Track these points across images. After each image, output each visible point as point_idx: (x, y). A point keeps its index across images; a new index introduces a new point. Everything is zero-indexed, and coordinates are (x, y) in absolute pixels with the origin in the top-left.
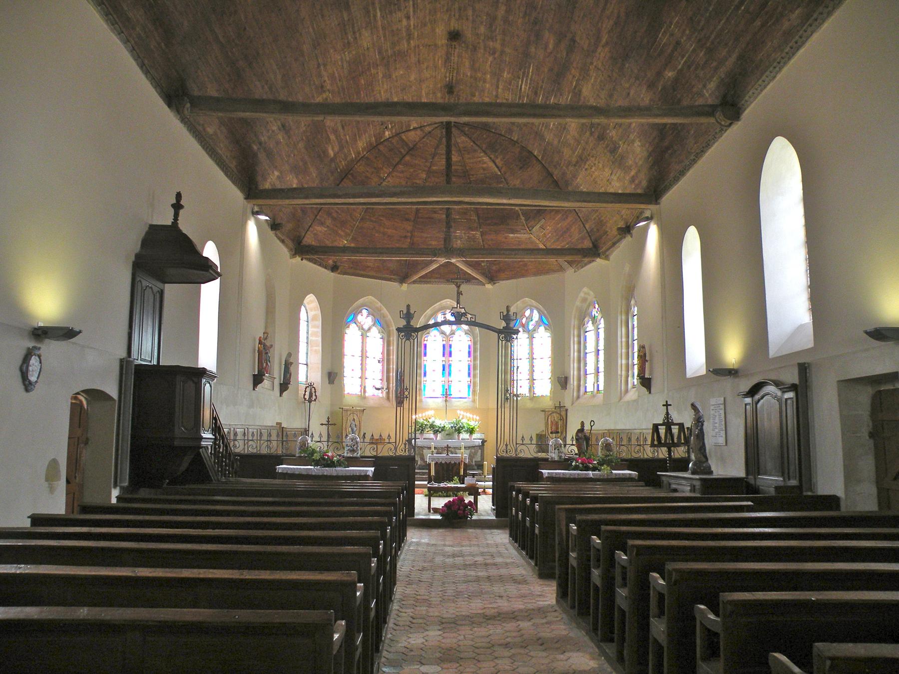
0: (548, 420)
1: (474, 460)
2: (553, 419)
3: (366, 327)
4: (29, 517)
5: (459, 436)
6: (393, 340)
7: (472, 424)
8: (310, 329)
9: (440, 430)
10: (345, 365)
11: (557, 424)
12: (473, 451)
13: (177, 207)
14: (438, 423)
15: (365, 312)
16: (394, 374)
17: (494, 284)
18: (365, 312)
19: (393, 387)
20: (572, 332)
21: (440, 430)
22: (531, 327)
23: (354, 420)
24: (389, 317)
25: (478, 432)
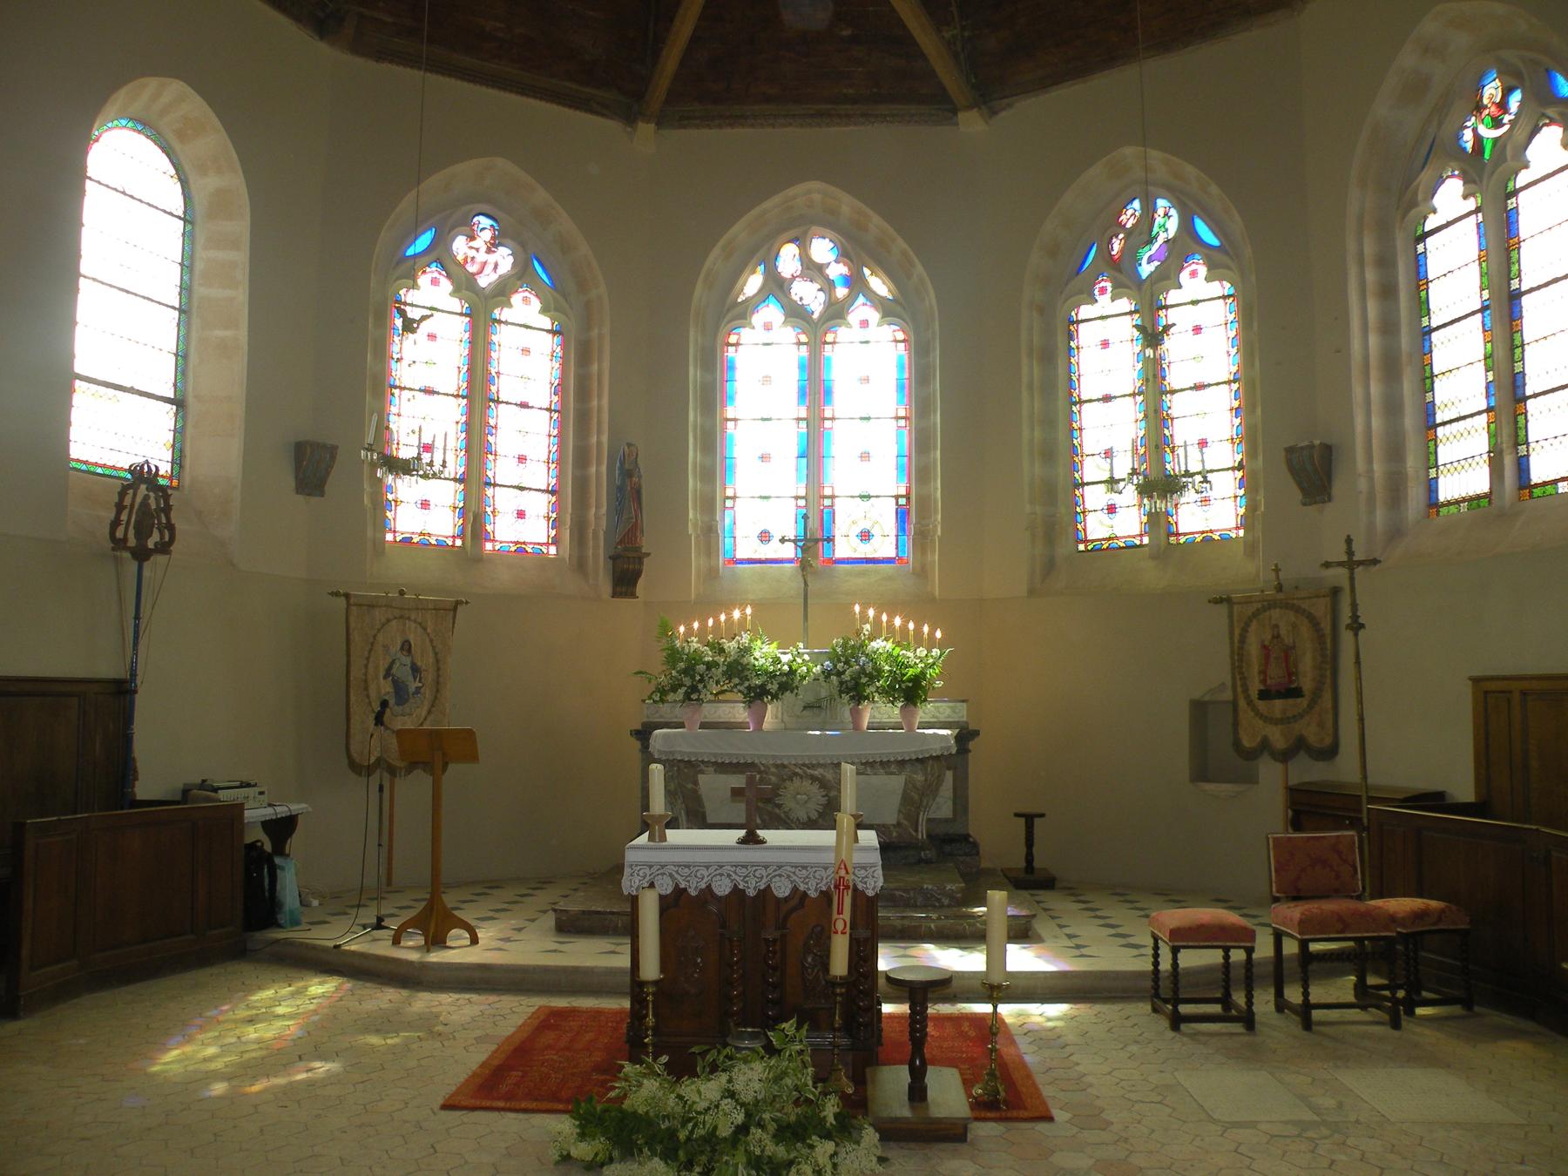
0: (1243, 640)
1: (922, 818)
2: (1268, 636)
5: (856, 715)
6: (601, 337)
7: (917, 658)
8: (201, 254)
9: (774, 687)
10: (82, 253)
11: (1288, 656)
12: (920, 777)
13: (337, 594)
14: (764, 653)
16: (604, 468)
17: (994, 113)
19: (597, 517)
20: (1351, 246)
21: (774, 687)
22: (1146, 269)
23: (406, 647)
25: (942, 695)
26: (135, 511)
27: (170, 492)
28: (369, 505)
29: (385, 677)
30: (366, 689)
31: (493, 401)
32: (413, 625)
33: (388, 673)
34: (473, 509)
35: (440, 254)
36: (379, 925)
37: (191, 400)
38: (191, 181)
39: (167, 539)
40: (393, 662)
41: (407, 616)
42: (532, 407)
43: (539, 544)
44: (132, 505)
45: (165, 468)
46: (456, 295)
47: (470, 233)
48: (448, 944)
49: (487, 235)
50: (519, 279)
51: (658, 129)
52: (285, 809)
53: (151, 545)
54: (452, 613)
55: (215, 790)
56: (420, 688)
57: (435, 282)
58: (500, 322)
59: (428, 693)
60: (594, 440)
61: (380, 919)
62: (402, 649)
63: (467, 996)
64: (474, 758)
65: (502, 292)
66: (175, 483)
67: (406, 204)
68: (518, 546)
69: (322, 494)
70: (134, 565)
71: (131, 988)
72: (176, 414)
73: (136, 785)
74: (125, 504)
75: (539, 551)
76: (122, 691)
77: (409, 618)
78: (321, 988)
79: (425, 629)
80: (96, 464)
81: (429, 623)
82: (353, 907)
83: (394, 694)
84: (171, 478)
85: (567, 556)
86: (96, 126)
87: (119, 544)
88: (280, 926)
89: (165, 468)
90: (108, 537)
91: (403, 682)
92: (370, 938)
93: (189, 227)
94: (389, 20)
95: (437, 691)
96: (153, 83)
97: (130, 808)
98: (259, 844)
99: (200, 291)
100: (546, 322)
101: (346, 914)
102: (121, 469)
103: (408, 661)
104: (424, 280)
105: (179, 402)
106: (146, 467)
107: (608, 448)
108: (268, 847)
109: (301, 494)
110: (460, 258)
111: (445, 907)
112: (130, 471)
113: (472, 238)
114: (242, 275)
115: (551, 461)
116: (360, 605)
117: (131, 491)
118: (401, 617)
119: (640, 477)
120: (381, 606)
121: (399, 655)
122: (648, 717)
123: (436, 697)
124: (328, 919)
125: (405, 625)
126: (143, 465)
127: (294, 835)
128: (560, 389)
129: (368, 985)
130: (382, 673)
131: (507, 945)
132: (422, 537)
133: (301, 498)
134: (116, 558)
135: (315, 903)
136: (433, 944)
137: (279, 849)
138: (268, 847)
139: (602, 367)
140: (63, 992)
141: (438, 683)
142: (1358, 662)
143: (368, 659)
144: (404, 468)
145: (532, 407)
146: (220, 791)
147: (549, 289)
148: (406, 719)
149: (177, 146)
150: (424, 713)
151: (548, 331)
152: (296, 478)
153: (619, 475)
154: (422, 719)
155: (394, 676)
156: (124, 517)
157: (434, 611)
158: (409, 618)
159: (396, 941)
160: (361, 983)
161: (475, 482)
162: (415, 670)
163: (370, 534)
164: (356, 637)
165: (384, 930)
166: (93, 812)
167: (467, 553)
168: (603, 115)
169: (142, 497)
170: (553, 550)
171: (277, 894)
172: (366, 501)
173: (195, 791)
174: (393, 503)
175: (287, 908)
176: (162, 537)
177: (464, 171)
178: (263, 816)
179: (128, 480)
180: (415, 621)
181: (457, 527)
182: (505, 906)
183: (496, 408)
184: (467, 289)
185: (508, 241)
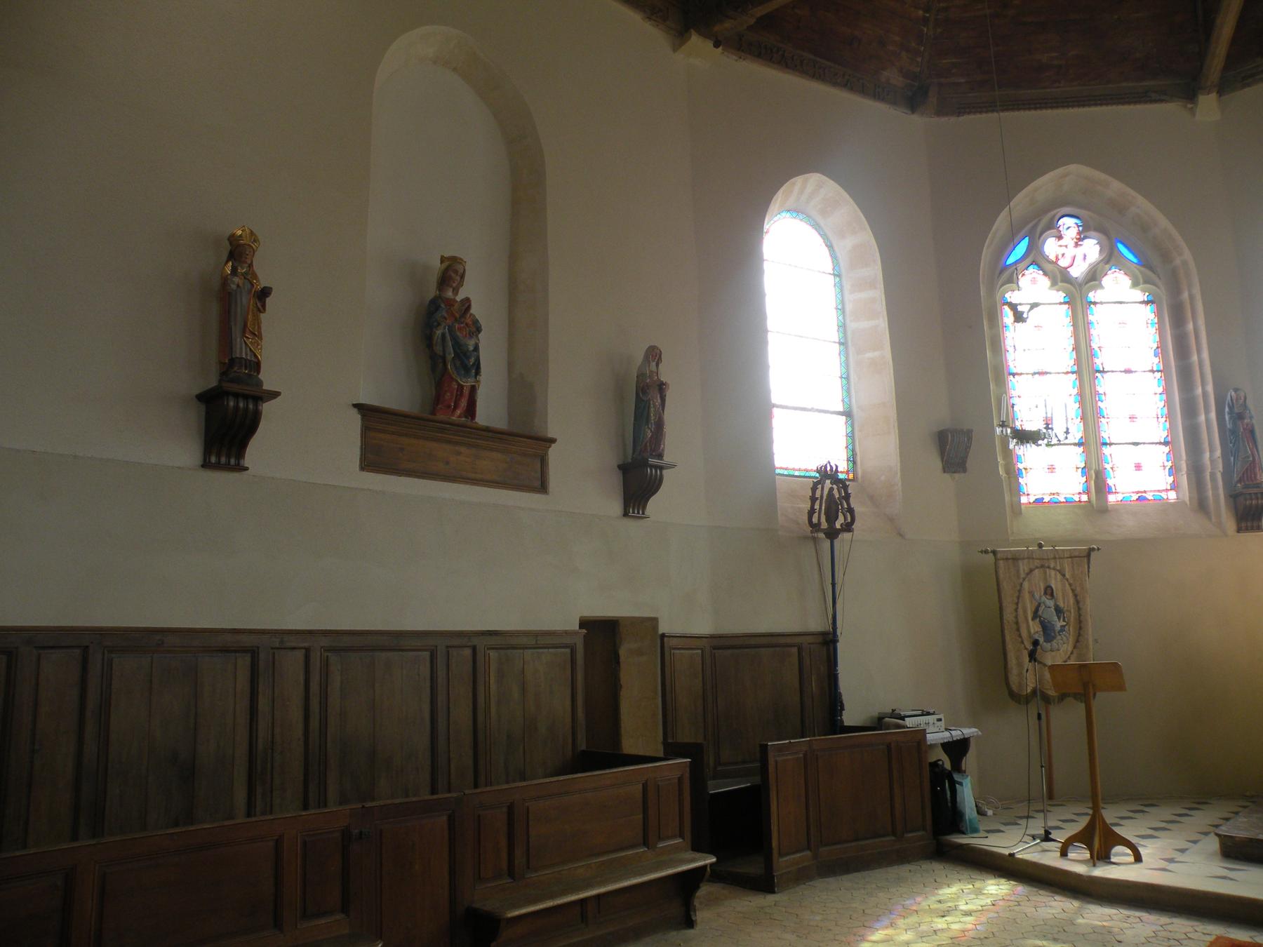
3: (1077, 271)
4: (247, 469)
6: (1192, 297)
8: (847, 296)
13: (986, 552)
15: (1069, 226)
16: (1213, 415)
18: (1069, 226)
19: (1212, 461)
23: (1049, 591)
24: (1163, 222)
26: (824, 501)
27: (847, 483)
28: (1004, 475)
29: (1033, 619)
30: (1018, 630)
31: (1099, 371)
32: (1053, 573)
33: (1036, 615)
34: (1094, 468)
35: (1035, 257)
36: (1047, 838)
37: (855, 410)
38: (835, 245)
39: (849, 520)
40: (1039, 605)
41: (1046, 565)
42: (1136, 372)
43: (1159, 491)
44: (822, 496)
45: (843, 466)
46: (1053, 288)
47: (1057, 234)
48: (1113, 859)
49: (1073, 232)
50: (1107, 262)
51: (1220, 96)
52: (959, 733)
53: (838, 526)
54: (1086, 560)
55: (903, 718)
56: (1064, 626)
57: (1034, 281)
58: (1095, 303)
59: (1072, 629)
60: (1199, 391)
61: (1047, 833)
62: (1045, 593)
63: (1138, 914)
64: (1121, 688)
65: (1094, 277)
66: (851, 476)
67: (1001, 223)
68: (1140, 495)
69: (965, 471)
70: (827, 543)
71: (850, 876)
72: (846, 423)
73: (843, 714)
74: (817, 496)
75: (1160, 498)
76: (829, 641)
77: (1049, 567)
78: (996, 888)
80: (794, 469)
81: (1067, 570)
82: (1021, 818)
83: (1042, 633)
84: (847, 472)
85: (1187, 499)
86: (766, 222)
87: (815, 527)
88: (963, 833)
89: (843, 466)
90: (807, 522)
91: (1049, 622)
92: (1040, 849)
93: (838, 279)
94: (962, 80)
95: (1080, 628)
96: (799, 180)
97: (801, 738)
98: (940, 763)
99: (852, 326)
100: (1139, 295)
101: (1017, 824)
102: (811, 470)
103: (1051, 603)
104: (1024, 281)
105: (848, 414)
106: (828, 466)
107: (1215, 398)
108: (948, 766)
109: (948, 472)
110: (1053, 258)
111: (1104, 822)
112: (818, 471)
113: (1060, 237)
114: (881, 307)
115: (1160, 416)
116: (1007, 559)
117: (820, 486)
119: (1251, 418)
120: (1024, 559)
121: (1044, 598)
123: (1079, 635)
124: (1002, 829)
125: (1045, 573)
126: (826, 466)
127: (968, 755)
128: (1161, 349)
129: (1041, 892)
131: (1171, 866)
133: (947, 476)
134: (814, 539)
135: (990, 813)
136: (1098, 859)
137: (957, 766)
138: (948, 766)
139: (1197, 325)
140: (802, 876)
141: (1080, 622)
143: (1017, 604)
144: (1026, 437)
145: (1136, 372)
146: (906, 719)
147: (1135, 265)
148: (1059, 653)
149: (822, 222)
150: (1070, 649)
151: (1143, 302)
152: (942, 460)
153: (1230, 418)
154: (1069, 653)
155: (1040, 617)
156: (817, 507)
157: (1070, 559)
158: (1049, 567)
159: (1064, 854)
160: (1035, 890)
161: (1092, 444)
162: (1059, 611)
163: (1007, 498)
164: (1006, 586)
165: (1053, 842)
166: (814, 736)
167: (1093, 506)
168: (1161, 101)
169: (827, 490)
170: (1172, 496)
171: (958, 805)
172: (1001, 471)
173: (887, 719)
174: (1023, 470)
175: (967, 818)
176: (845, 518)
177: (1043, 186)
178: (942, 738)
179: (817, 478)
182: (1163, 825)
183: (1103, 377)
184: (1063, 281)
185: (1092, 233)
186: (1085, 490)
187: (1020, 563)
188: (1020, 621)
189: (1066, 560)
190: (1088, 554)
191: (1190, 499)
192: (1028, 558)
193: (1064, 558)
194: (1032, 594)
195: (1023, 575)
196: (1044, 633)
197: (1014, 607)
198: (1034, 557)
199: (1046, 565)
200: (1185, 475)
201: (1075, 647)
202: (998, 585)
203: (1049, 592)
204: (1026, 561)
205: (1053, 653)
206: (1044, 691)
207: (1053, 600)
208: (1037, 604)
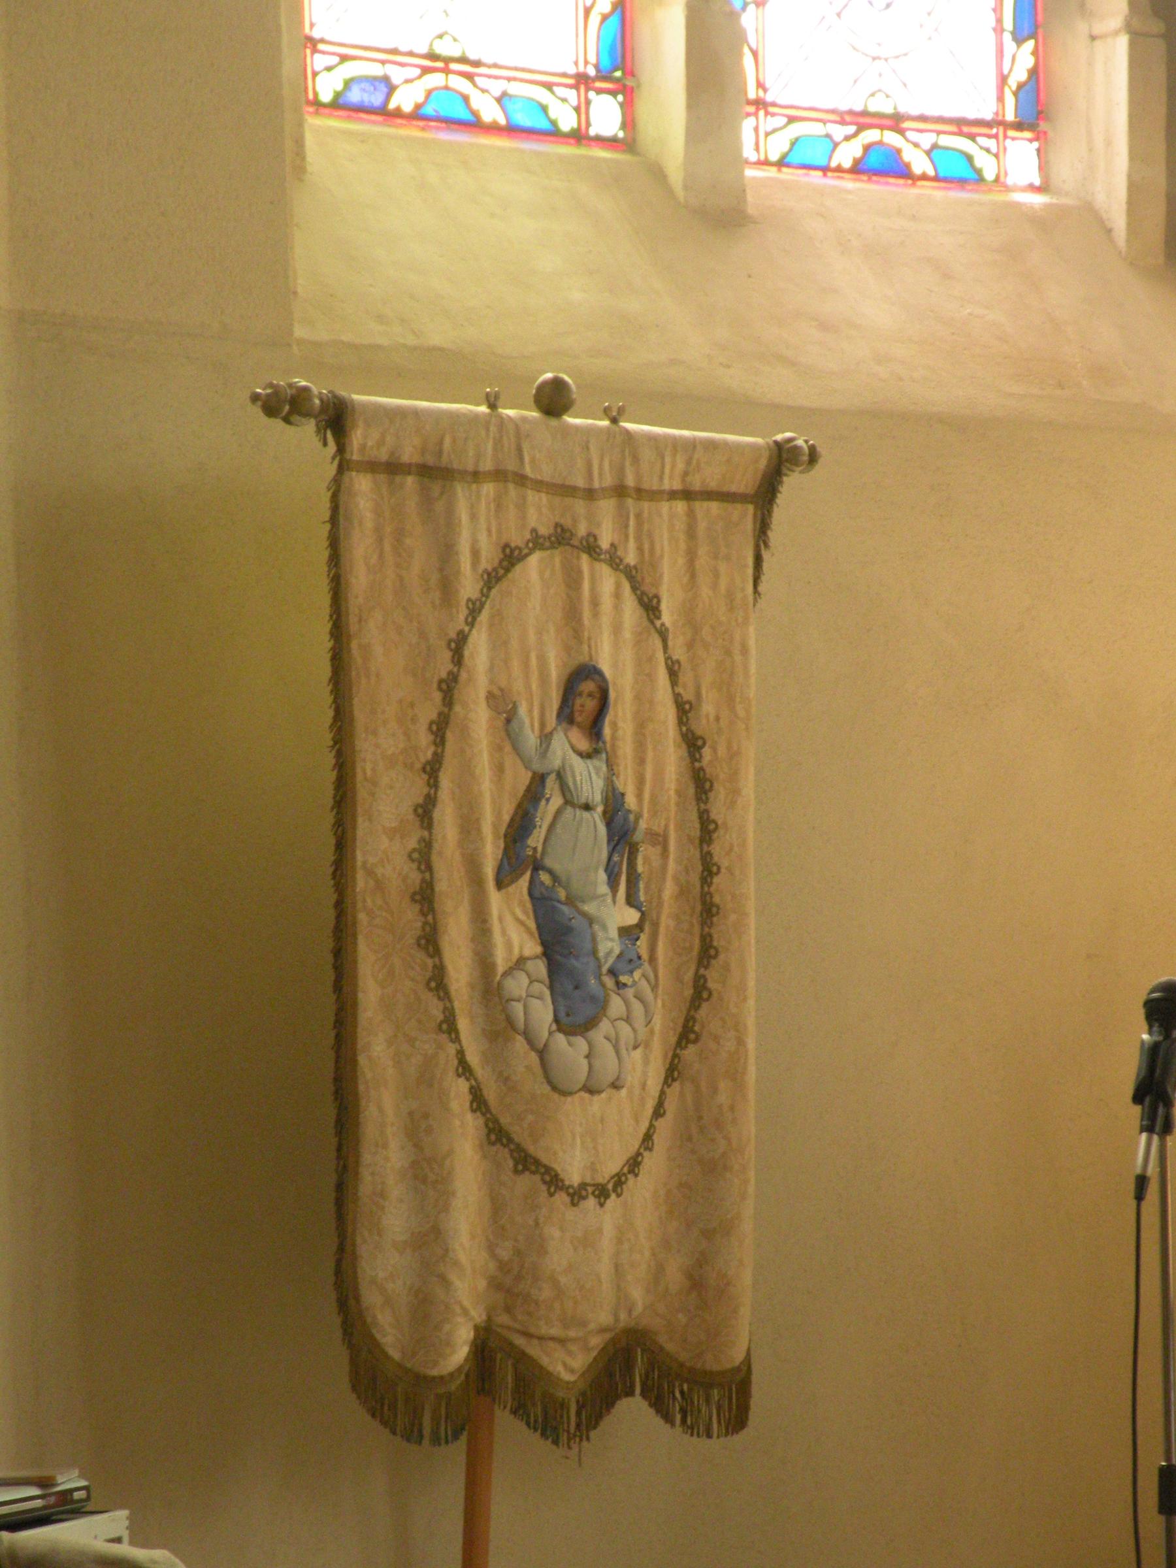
30: (430, 941)
32: (605, 570)
40: (534, 794)
41: (582, 530)
54: (747, 514)
68: (872, 135)
69: (1031, 54)
77: (591, 547)
79: (650, 607)
83: (540, 968)
95: (707, 953)
118: (561, 537)
120: (476, 476)
122: (499, 838)
123: (700, 992)
125: (572, 580)
130: (491, 853)
132: (437, 79)
141: (708, 911)
142: (757, 18)
143: (432, 770)
157: (680, 506)
167: (658, 173)
180: (615, 562)
181: (595, 19)
186: (606, 63)
187: (461, 492)
188: (441, 886)
189: (665, 507)
190: (660, 516)
191: (1134, 188)
192: (499, 475)
193: (654, 495)
194: (507, 717)
195: (468, 587)
196: (554, 968)
197: (417, 789)
198: (528, 470)
199: (582, 530)
200: (1122, 43)
201: (672, 1073)
202: (339, 631)
203: (586, 705)
204: (488, 489)
205: (596, 1104)
206: (533, 1350)
207: (600, 763)
208: (525, 778)
